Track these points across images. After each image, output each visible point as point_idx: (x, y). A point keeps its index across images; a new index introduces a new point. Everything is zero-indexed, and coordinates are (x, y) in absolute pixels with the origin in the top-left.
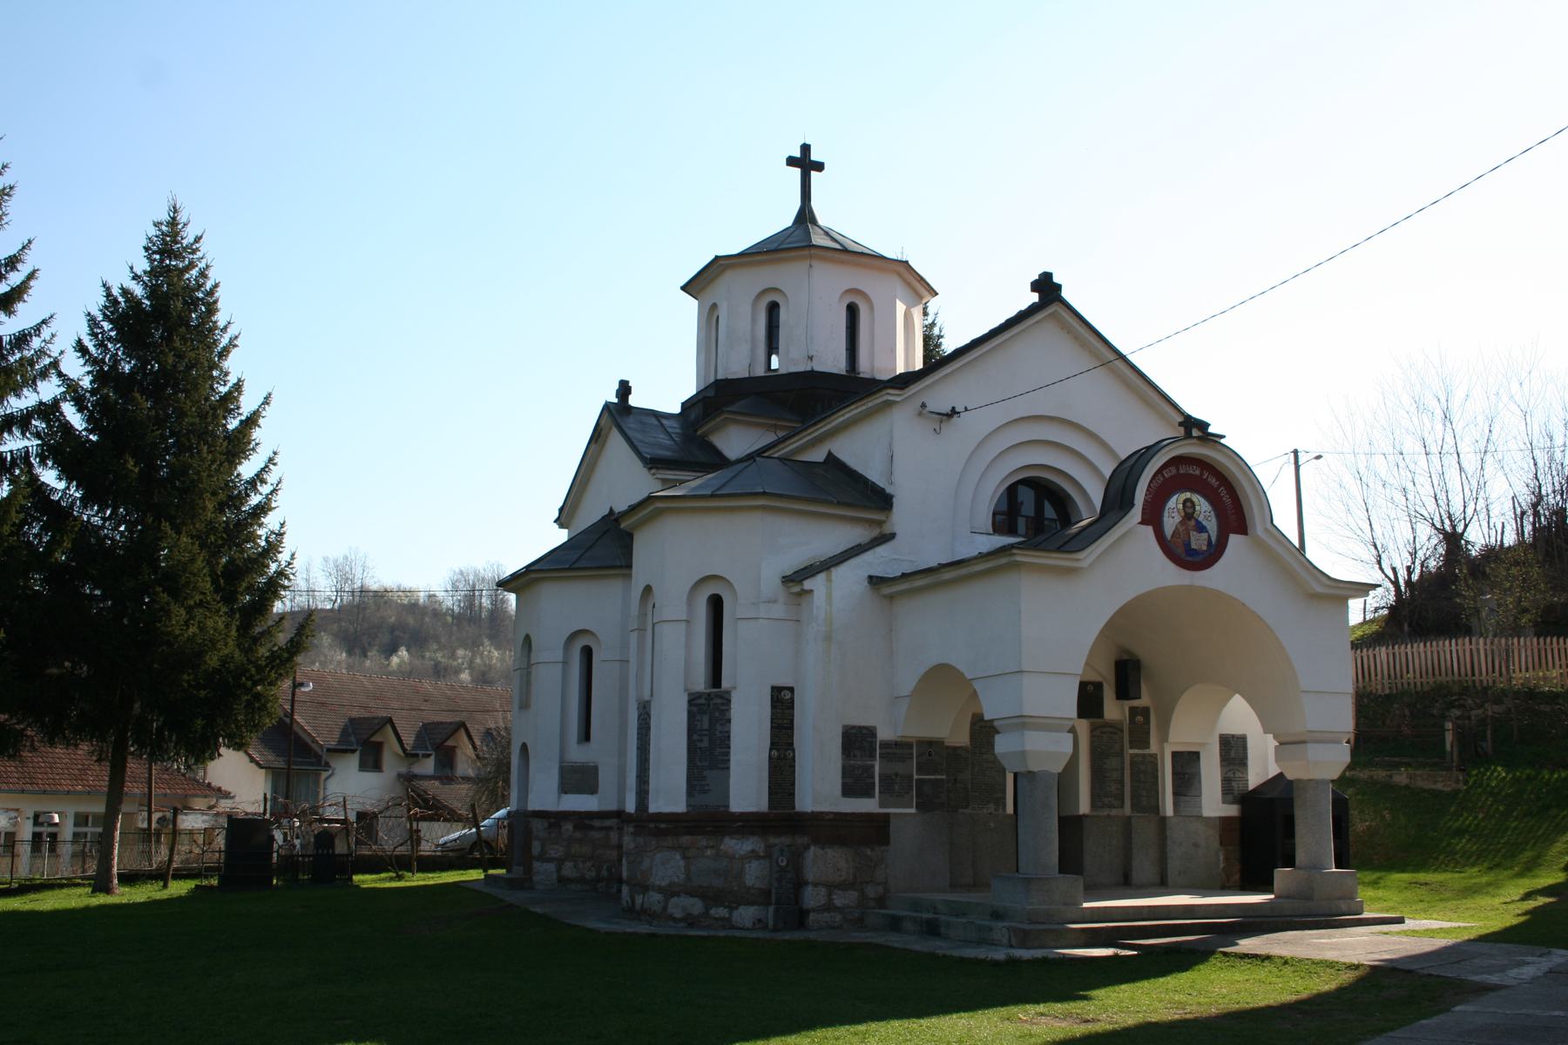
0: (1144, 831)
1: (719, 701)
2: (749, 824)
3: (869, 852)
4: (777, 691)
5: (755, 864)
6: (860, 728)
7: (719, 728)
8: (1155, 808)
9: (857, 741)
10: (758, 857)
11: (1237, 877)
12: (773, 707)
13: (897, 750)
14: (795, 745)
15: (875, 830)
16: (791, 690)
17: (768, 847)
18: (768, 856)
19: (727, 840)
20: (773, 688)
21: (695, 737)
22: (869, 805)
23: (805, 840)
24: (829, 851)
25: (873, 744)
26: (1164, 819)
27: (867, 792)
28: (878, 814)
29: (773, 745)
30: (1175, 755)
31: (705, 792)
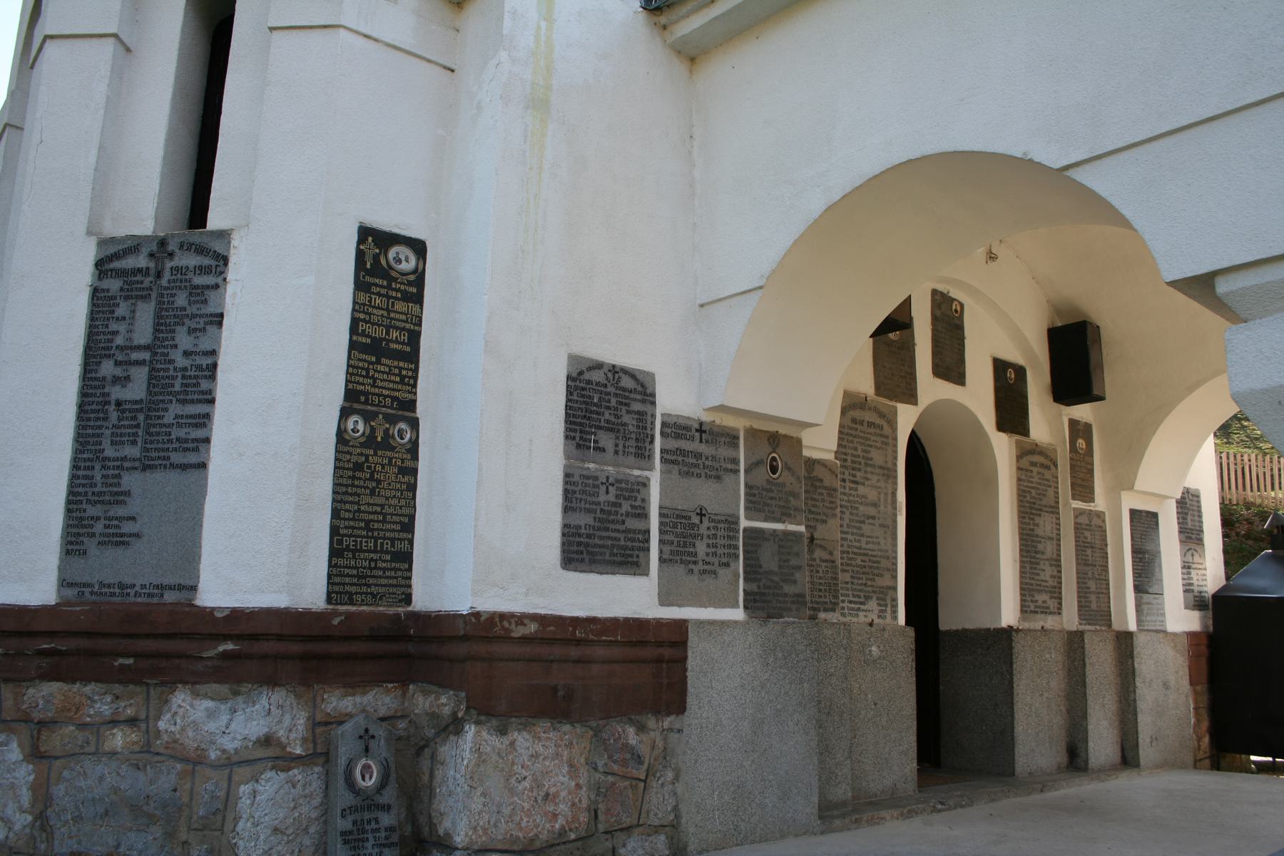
0: (1100, 659)
1: (191, 260)
2: (263, 648)
3: (632, 735)
4: (374, 243)
5: (271, 785)
6: (616, 371)
7: (184, 340)
8: (1104, 617)
9: (603, 404)
10: (284, 761)
11: (1206, 739)
12: (360, 286)
13: (700, 445)
14: (422, 411)
15: (648, 667)
16: (419, 248)
17: (322, 726)
18: (320, 753)
19: (181, 698)
20: (365, 233)
21: (107, 368)
22: (629, 597)
23: (445, 703)
24: (522, 740)
25: (644, 421)
26: (1129, 635)
27: (627, 559)
28: (659, 624)
29: (354, 400)
30: (1133, 513)
31: (120, 541)
